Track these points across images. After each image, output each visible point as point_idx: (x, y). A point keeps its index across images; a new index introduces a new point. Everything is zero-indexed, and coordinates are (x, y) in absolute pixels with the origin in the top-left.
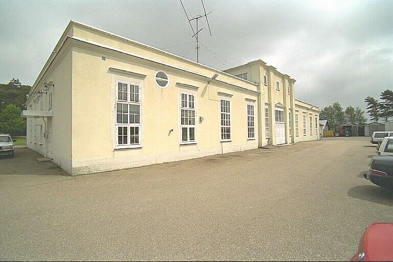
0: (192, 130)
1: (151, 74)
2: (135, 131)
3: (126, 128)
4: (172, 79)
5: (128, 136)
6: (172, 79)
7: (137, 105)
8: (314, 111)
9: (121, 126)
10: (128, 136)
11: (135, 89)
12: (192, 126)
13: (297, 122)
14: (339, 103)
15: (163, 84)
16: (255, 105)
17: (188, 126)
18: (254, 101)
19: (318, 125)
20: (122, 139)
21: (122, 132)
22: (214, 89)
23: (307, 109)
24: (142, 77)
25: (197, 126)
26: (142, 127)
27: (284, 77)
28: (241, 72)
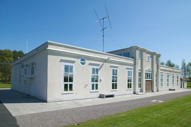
0: (97, 85)
1: (78, 61)
2: (71, 86)
3: (129, 83)
4: (87, 62)
5: (68, 87)
6: (87, 62)
7: (72, 74)
8: (175, 72)
9: (96, 83)
10: (68, 87)
11: (116, 70)
12: (71, 83)
13: (162, 79)
14: (22, 51)
15: (83, 64)
16: (132, 71)
17: (95, 83)
18: (131, 69)
19: (179, 79)
20: (93, 88)
21: (66, 86)
22: (108, 65)
23: (171, 71)
24: (73, 62)
25: (98, 83)
26: (73, 83)
27: (152, 54)
28: (127, 53)
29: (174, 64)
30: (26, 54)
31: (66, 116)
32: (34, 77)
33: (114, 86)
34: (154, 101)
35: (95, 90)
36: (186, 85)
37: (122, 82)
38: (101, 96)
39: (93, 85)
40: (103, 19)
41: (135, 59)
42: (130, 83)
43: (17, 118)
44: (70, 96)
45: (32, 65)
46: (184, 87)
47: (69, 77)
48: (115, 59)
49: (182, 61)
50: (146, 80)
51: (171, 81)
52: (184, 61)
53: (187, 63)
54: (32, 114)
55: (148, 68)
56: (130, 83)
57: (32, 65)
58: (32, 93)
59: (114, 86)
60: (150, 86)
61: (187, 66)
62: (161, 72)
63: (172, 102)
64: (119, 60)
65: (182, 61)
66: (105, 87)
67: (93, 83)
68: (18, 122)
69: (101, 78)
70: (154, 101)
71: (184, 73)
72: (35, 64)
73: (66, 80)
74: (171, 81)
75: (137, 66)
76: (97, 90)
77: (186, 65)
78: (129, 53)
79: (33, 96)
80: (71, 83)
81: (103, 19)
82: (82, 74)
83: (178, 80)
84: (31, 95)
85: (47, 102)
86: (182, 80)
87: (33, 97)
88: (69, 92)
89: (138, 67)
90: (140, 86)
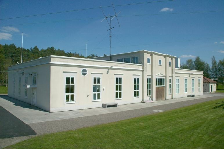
0: (99, 95)
20: (95, 98)
21: (67, 97)
29: (203, 62)
30: (12, 34)
31: (67, 124)
32: (36, 87)
33: (118, 95)
34: (155, 111)
35: (97, 100)
36: (214, 87)
37: (127, 88)
38: (104, 106)
39: (95, 95)
40: (111, 17)
41: (143, 65)
42: (136, 91)
43: (30, 126)
44: (71, 106)
45: (35, 75)
46: (213, 91)
47: (71, 88)
48: (119, 66)
49: (213, 59)
50: (156, 87)
51: (190, 85)
52: (214, 59)
53: (218, 62)
54: (40, 123)
55: (160, 73)
56: (136, 90)
57: (35, 75)
58: (35, 102)
59: (118, 95)
60: (160, 94)
61: (218, 64)
62: (177, 75)
63: (190, 108)
64: (124, 67)
65: (213, 59)
66: (108, 95)
67: (95, 93)
68: (32, 128)
69: (104, 88)
70: (155, 111)
71: (215, 73)
72: (38, 74)
73: (67, 91)
74: (190, 85)
75: (145, 72)
76: (99, 100)
77: (217, 64)
78: (137, 57)
79: (36, 105)
80: (72, 94)
81: (111, 17)
82: (83, 87)
83: (199, 84)
84: (33, 104)
85: (50, 112)
86: (210, 83)
87: (35, 107)
88: (70, 102)
89: (146, 73)
90: (149, 93)
